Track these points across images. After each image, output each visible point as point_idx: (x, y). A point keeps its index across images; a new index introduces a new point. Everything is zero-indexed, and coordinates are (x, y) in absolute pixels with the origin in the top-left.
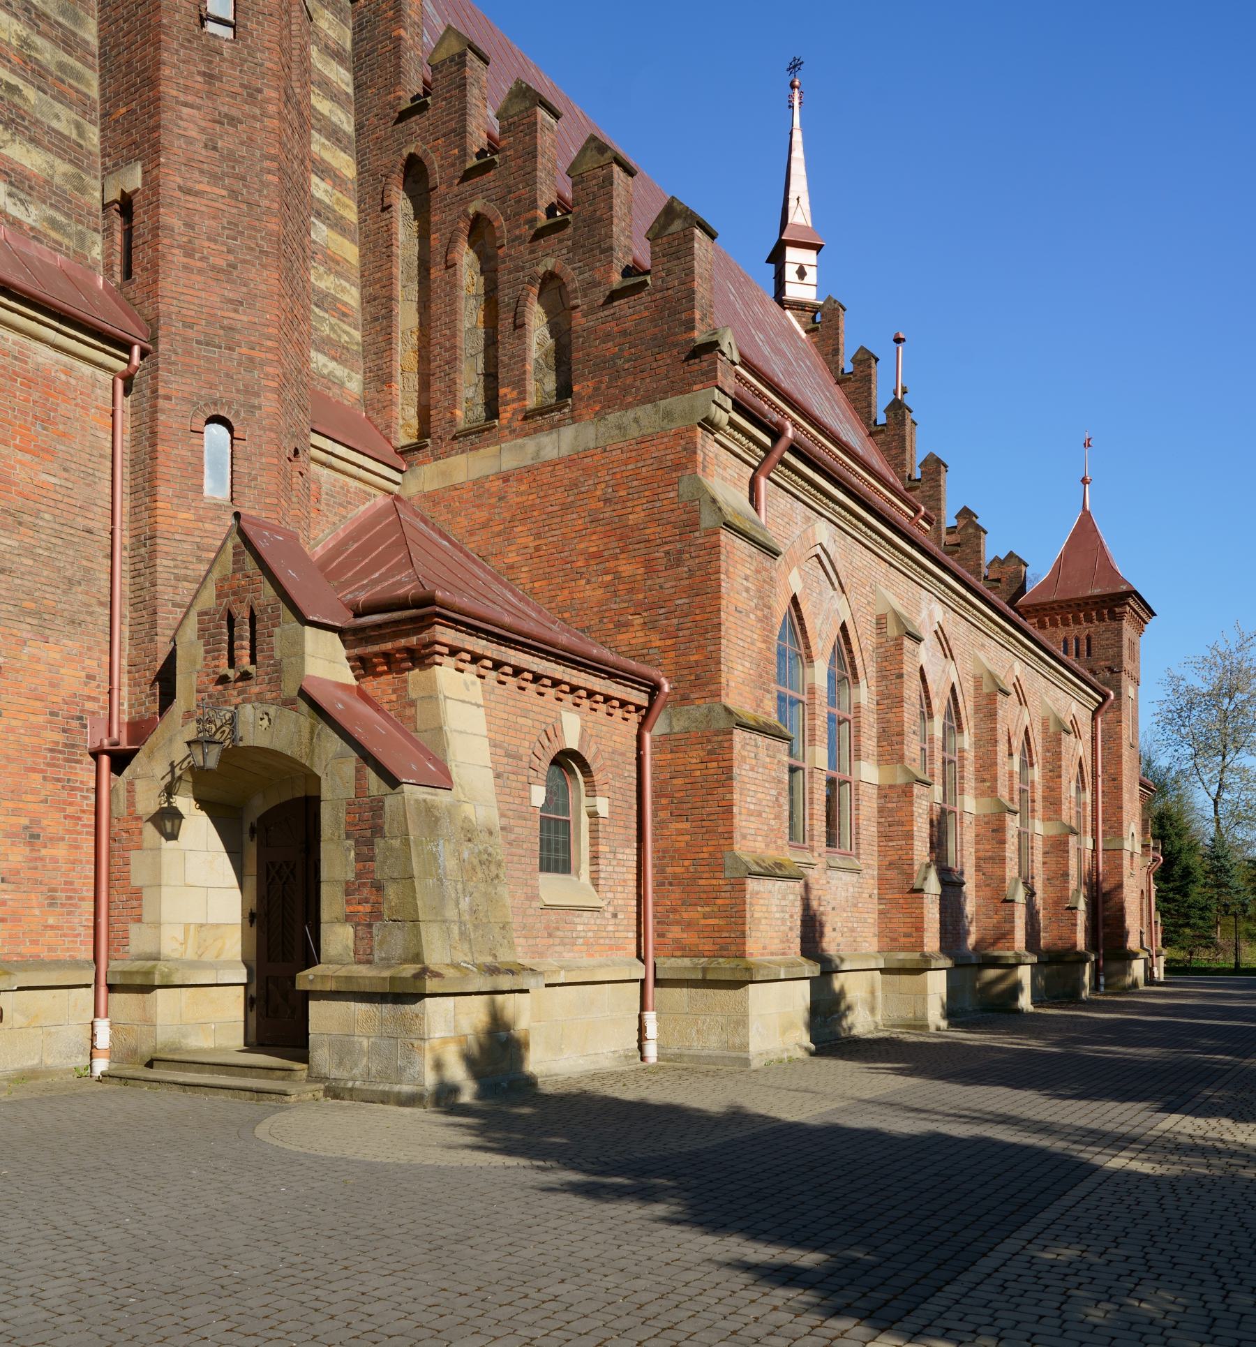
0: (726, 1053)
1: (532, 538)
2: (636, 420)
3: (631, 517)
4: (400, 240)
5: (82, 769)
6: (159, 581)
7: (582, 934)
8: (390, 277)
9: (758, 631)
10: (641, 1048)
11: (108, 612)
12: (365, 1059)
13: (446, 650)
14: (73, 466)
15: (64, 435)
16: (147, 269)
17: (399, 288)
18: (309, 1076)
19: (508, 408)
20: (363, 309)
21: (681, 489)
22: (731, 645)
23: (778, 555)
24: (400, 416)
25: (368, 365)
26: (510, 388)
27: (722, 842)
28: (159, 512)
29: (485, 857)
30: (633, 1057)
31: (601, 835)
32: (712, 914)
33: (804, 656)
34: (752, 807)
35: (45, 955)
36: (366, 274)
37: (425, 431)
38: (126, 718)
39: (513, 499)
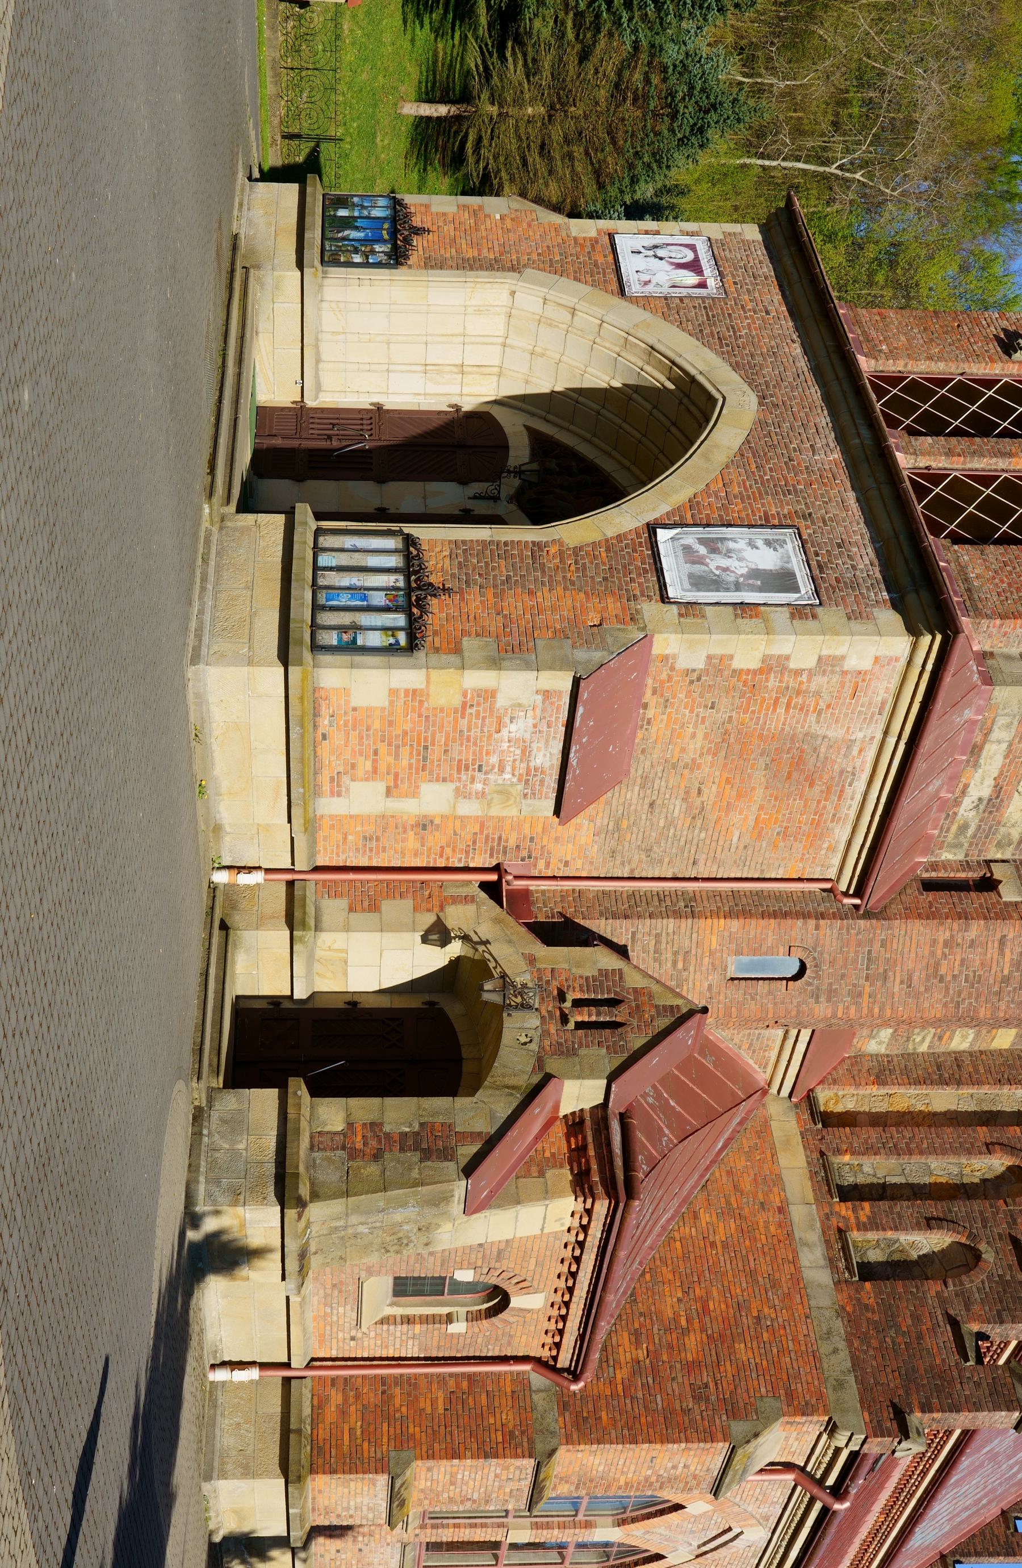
0: (217, 1454)
1: (724, 1239)
2: (835, 1351)
3: (742, 1345)
4: (1017, 1092)
5: (485, 858)
6: (654, 921)
7: (335, 1312)
8: (979, 1083)
9: (635, 1478)
10: (224, 1364)
11: (626, 875)
12: (227, 1146)
13: (588, 1206)
14: (750, 852)
15: (776, 846)
16: (930, 908)
17: (970, 1091)
18: (213, 1089)
19: (850, 1212)
20: (949, 1053)
21: (768, 1399)
22: (618, 1453)
23: (714, 1495)
24: (846, 1092)
25: (895, 1059)
26: (869, 1214)
27: (424, 1448)
28: (715, 921)
29: (405, 1242)
30: (215, 1357)
31: (430, 1326)
32: (353, 1438)
33: (624, 1516)
34: (460, 1476)
35: (321, 834)
36: (984, 1057)
37: (829, 1120)
38: (531, 888)
39: (761, 1218)
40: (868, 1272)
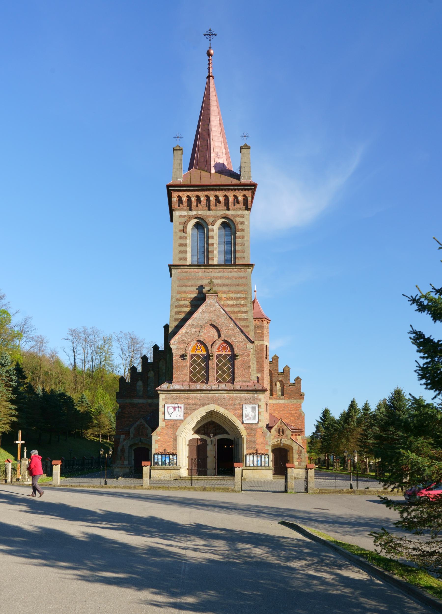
40: (283, 394)
